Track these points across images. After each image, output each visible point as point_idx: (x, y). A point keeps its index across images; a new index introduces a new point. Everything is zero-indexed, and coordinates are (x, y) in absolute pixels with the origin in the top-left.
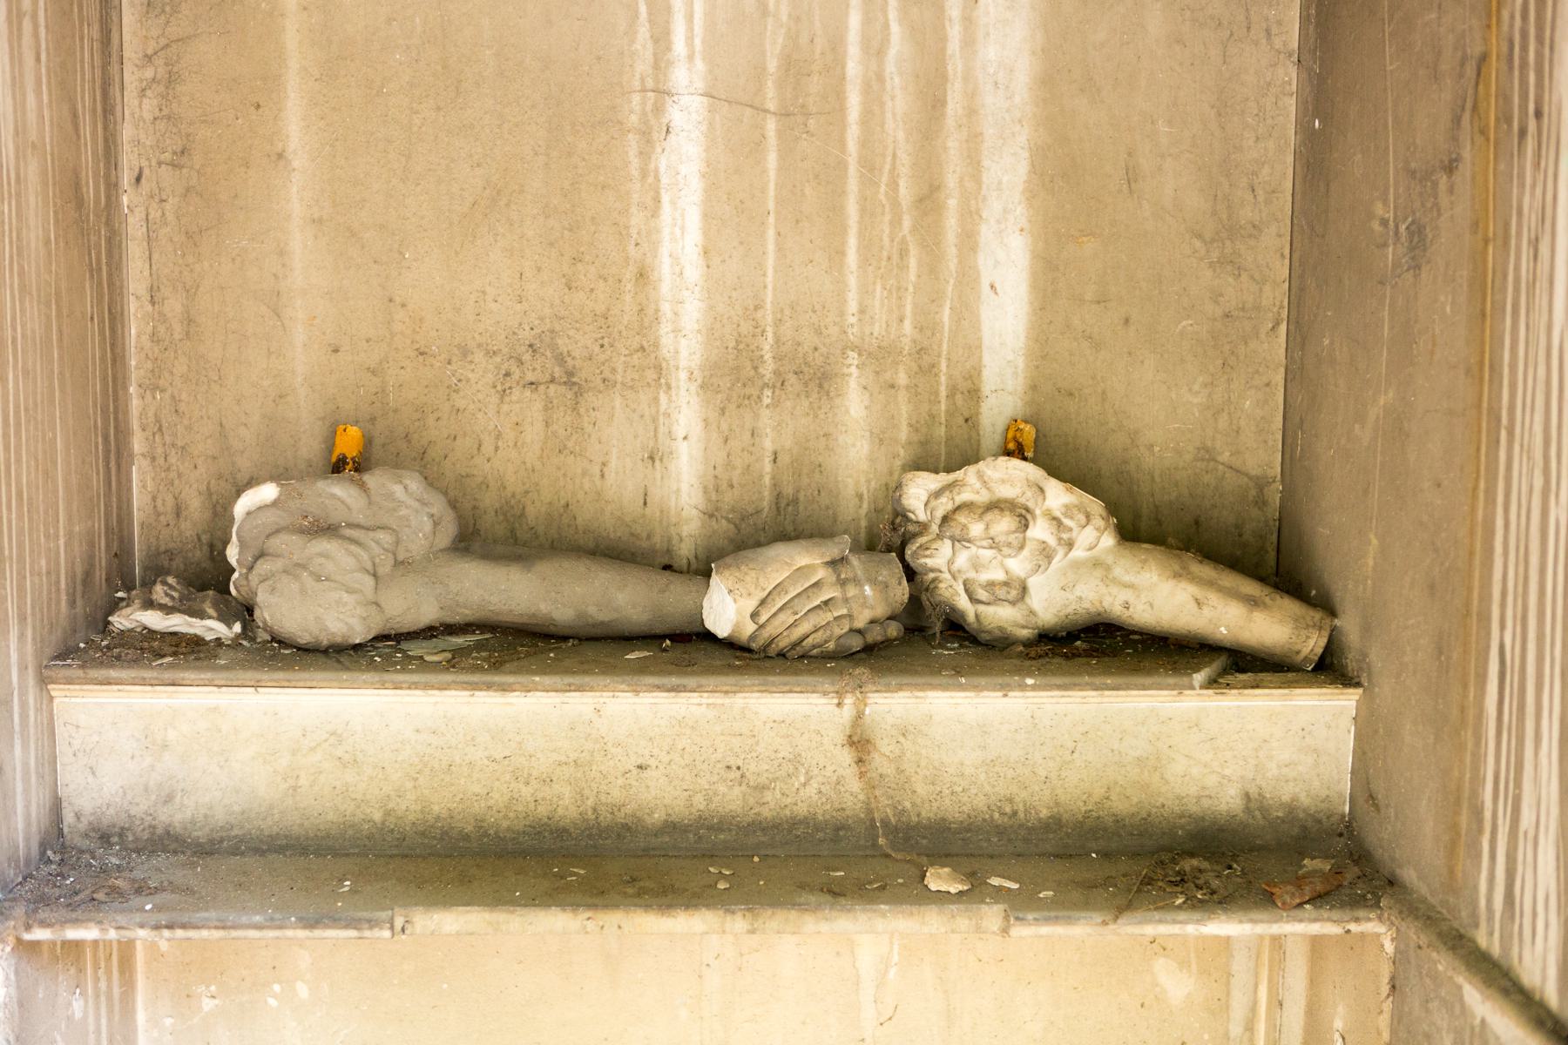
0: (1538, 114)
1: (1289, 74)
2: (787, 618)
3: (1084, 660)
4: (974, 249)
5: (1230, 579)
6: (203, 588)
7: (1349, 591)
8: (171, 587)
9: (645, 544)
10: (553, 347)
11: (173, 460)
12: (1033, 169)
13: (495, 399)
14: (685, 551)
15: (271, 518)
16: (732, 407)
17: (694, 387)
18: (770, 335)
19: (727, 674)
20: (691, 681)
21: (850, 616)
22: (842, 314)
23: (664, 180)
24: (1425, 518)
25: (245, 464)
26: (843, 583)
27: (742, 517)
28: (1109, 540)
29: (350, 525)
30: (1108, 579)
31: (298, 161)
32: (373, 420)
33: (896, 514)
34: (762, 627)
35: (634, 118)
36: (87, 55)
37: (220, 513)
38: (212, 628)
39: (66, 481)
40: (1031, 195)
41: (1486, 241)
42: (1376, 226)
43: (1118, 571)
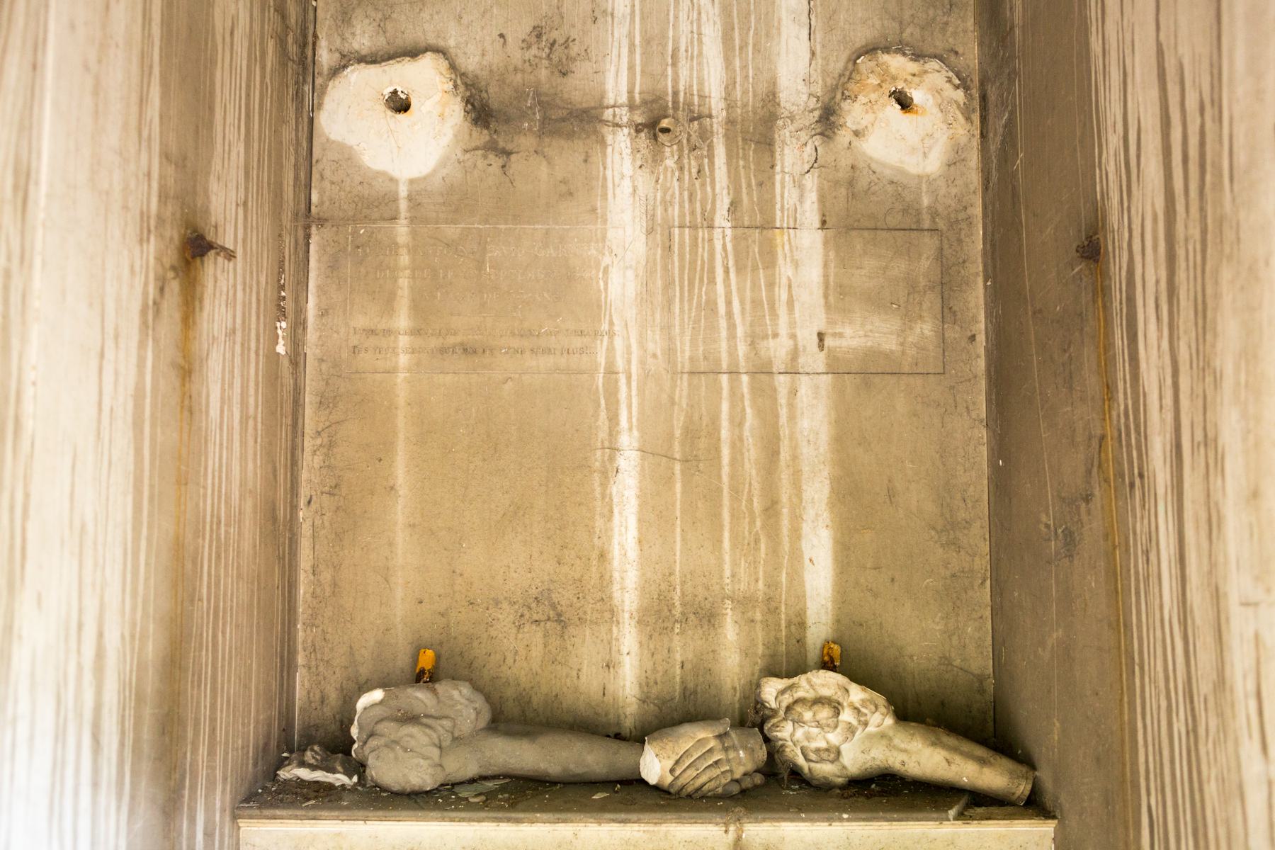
0: (1141, 476)
1: (982, 433)
2: (692, 773)
3: (877, 799)
4: (799, 538)
5: (968, 746)
6: (334, 752)
7: (1041, 753)
8: (316, 753)
9: (604, 720)
10: (549, 599)
11: (321, 669)
12: (833, 490)
13: (514, 630)
14: (628, 724)
15: (378, 712)
16: (656, 634)
17: (633, 623)
18: (678, 591)
19: (655, 812)
20: (634, 816)
21: (731, 771)
22: (721, 578)
23: (615, 500)
24: (1089, 713)
25: (364, 672)
26: (726, 749)
27: (663, 702)
28: (890, 721)
29: (426, 716)
30: (891, 746)
31: (402, 491)
32: (441, 644)
33: (757, 702)
34: (676, 778)
35: (597, 464)
36: (284, 434)
37: (348, 702)
38: (340, 779)
39: (257, 688)
40: (832, 505)
41: (1114, 549)
42: (1042, 527)
43: (897, 741)
